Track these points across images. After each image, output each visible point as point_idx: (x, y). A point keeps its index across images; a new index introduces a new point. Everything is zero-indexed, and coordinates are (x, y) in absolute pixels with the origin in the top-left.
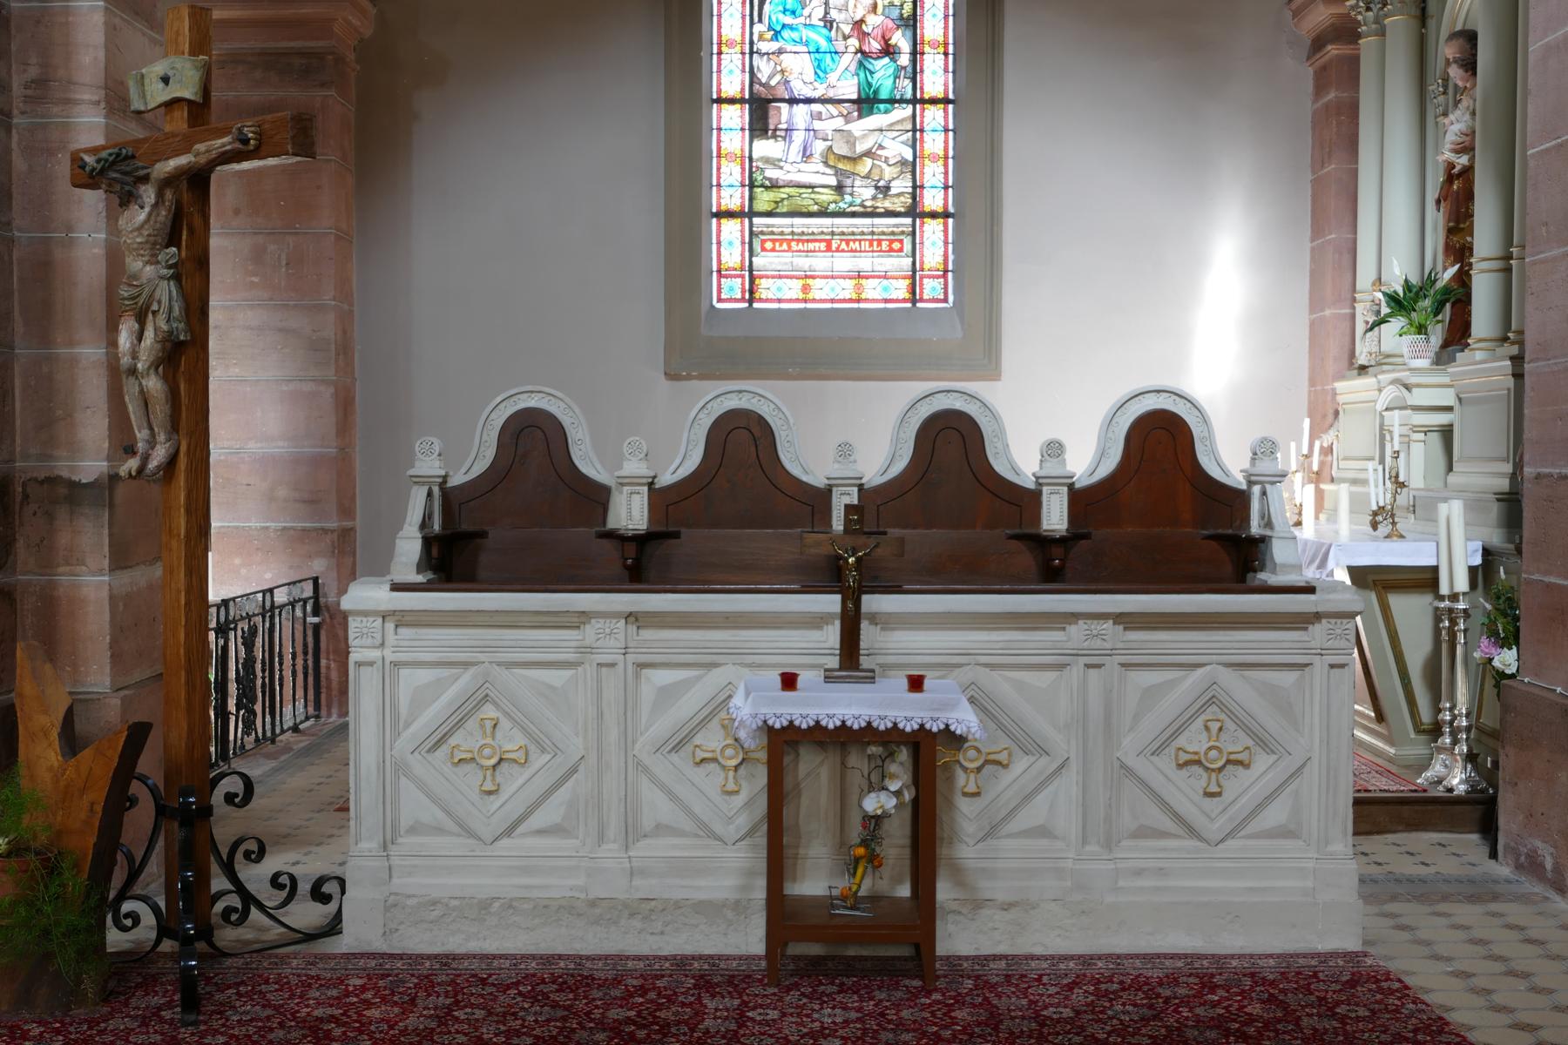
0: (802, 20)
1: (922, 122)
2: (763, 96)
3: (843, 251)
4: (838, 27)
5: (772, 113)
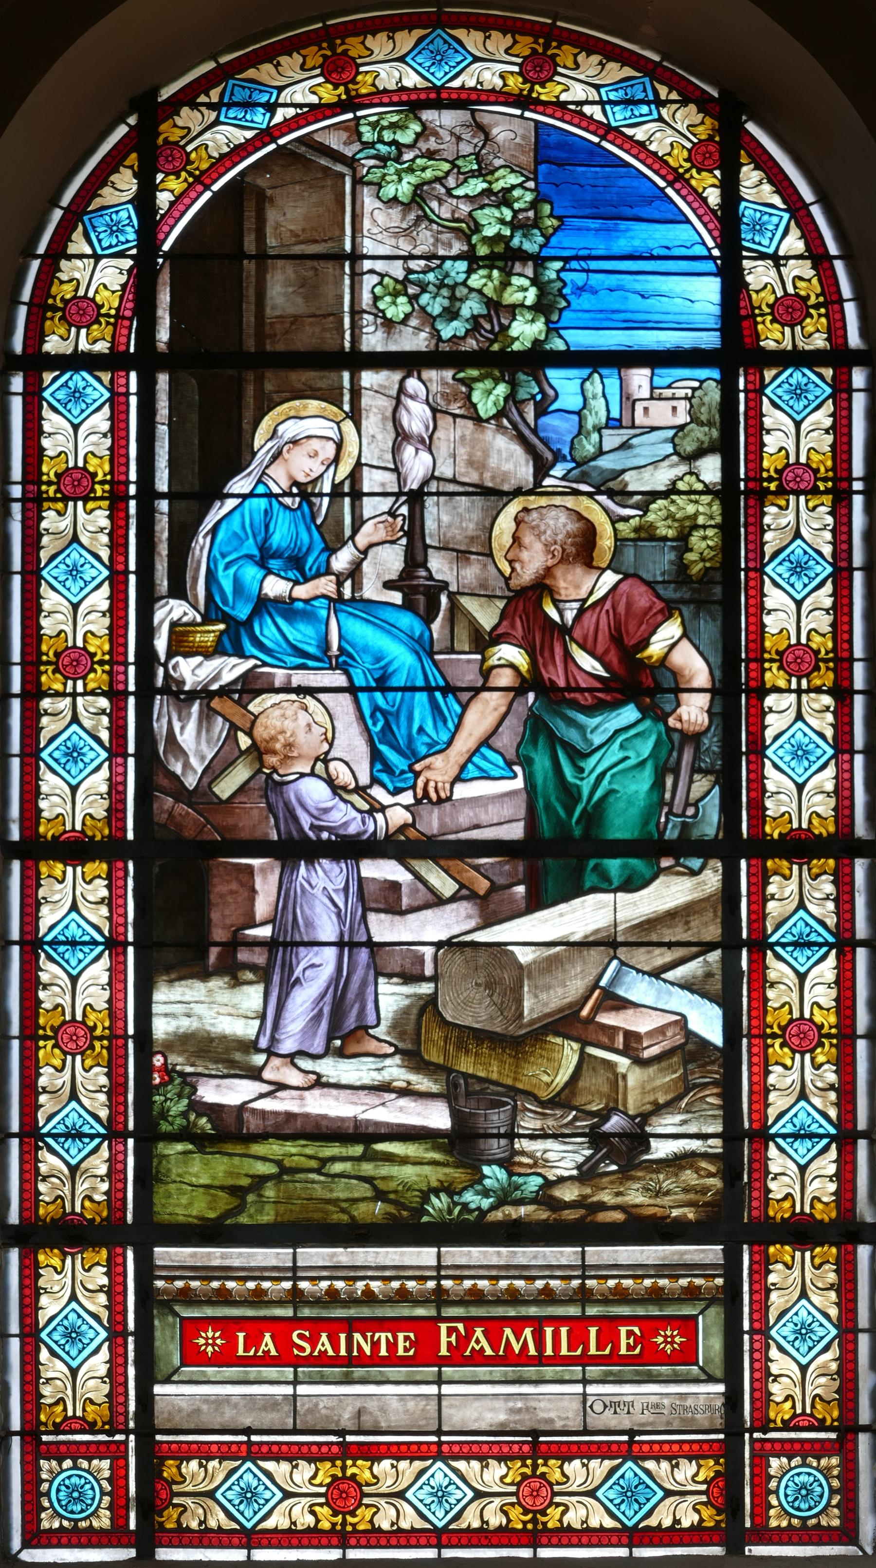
0: (326, 585)
1: (758, 915)
2: (189, 833)
3: (478, 1359)
4: (454, 608)
5: (220, 887)
